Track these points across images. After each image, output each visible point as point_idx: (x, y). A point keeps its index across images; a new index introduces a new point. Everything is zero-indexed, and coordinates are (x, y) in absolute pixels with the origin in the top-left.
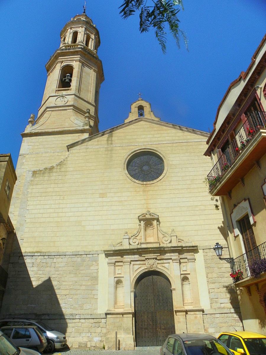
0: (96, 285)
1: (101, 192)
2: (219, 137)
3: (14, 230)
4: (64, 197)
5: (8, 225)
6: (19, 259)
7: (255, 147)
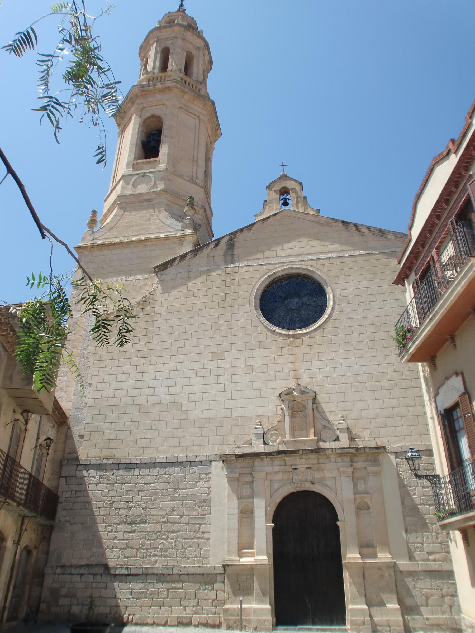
0: (208, 514)
1: (215, 349)
2: (416, 254)
3: (145, 185)
4: (150, 361)
5: (57, 412)
6: (76, 470)
7: (465, 287)
